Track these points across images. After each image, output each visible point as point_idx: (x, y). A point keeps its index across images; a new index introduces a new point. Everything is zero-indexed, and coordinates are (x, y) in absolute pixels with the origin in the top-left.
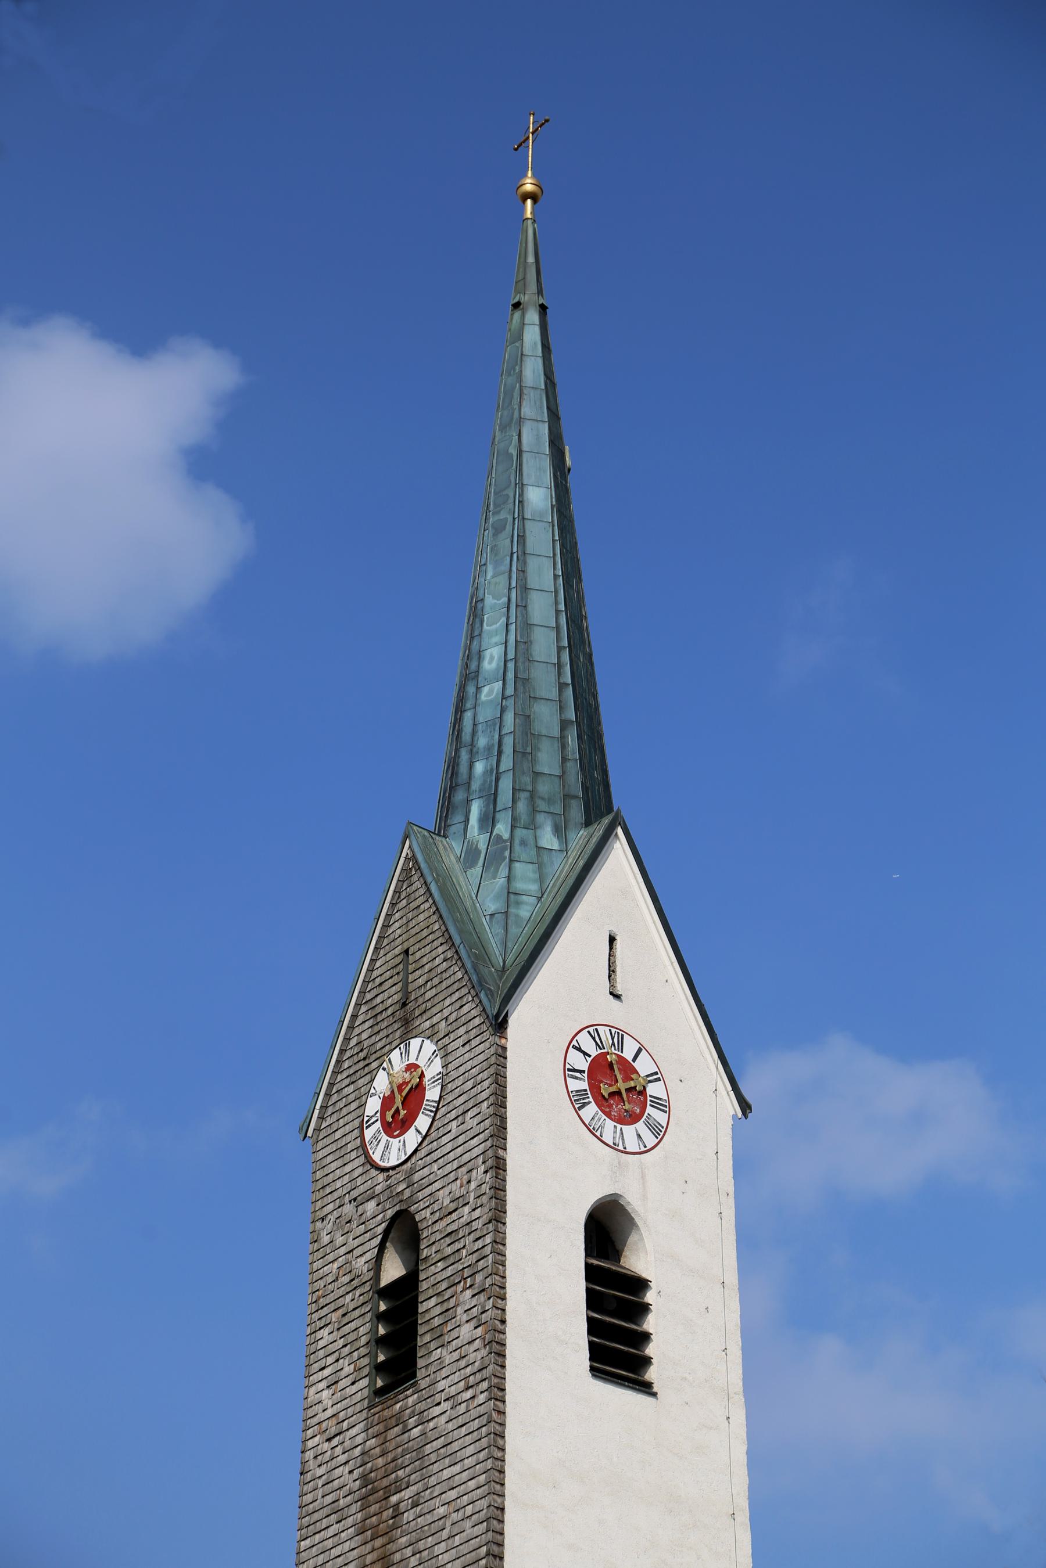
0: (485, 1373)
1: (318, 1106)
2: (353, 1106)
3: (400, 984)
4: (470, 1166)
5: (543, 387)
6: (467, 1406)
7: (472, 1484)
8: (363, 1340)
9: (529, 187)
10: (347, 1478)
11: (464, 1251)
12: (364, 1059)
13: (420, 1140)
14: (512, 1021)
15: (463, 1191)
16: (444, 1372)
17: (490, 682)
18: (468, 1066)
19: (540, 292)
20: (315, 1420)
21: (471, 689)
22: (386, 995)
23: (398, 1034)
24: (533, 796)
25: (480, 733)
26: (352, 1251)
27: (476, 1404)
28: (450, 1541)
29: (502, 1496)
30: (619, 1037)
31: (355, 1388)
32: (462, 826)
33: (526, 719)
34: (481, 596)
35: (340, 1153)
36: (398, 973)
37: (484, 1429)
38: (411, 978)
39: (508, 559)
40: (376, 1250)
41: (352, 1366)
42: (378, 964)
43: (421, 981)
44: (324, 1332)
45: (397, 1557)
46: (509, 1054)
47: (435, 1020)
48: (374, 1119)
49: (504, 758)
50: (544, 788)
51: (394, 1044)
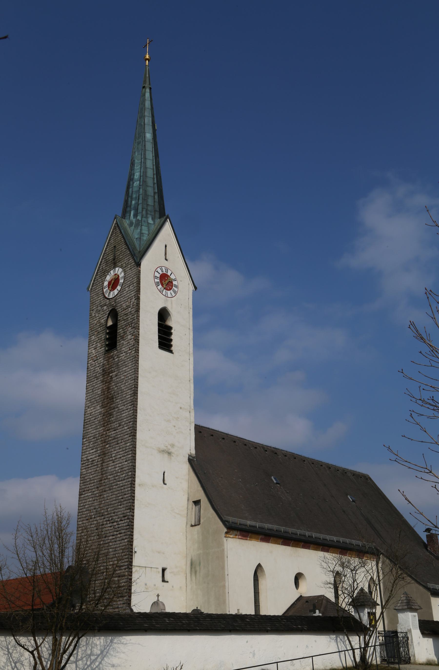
0: (134, 346)
1: (92, 283)
2: (101, 284)
3: (113, 255)
4: (131, 298)
5: (150, 108)
6: (130, 354)
7: (131, 371)
8: (103, 339)
9: (147, 57)
10: (99, 370)
11: (129, 318)
12: (104, 272)
13: (118, 292)
14: (142, 264)
15: (129, 304)
16: (124, 346)
17: (136, 181)
18: (131, 274)
19: (150, 84)
20: (91, 357)
21: (131, 183)
22: (109, 257)
23: (112, 266)
24: (147, 210)
25: (134, 194)
26: (100, 318)
27: (132, 353)
28: (125, 384)
29: (138, 374)
30: (167, 270)
31: (101, 350)
32: (129, 217)
33: (145, 191)
34: (134, 160)
35: (97, 295)
36: (113, 252)
37: (134, 359)
38: (116, 253)
39: (141, 151)
40: (106, 318)
41: (100, 345)
42: (107, 249)
43: (119, 254)
44: (93, 337)
45: (112, 387)
46: (141, 272)
47: (122, 263)
48: (106, 287)
49: (140, 200)
50: (149, 208)
51: (112, 269)
